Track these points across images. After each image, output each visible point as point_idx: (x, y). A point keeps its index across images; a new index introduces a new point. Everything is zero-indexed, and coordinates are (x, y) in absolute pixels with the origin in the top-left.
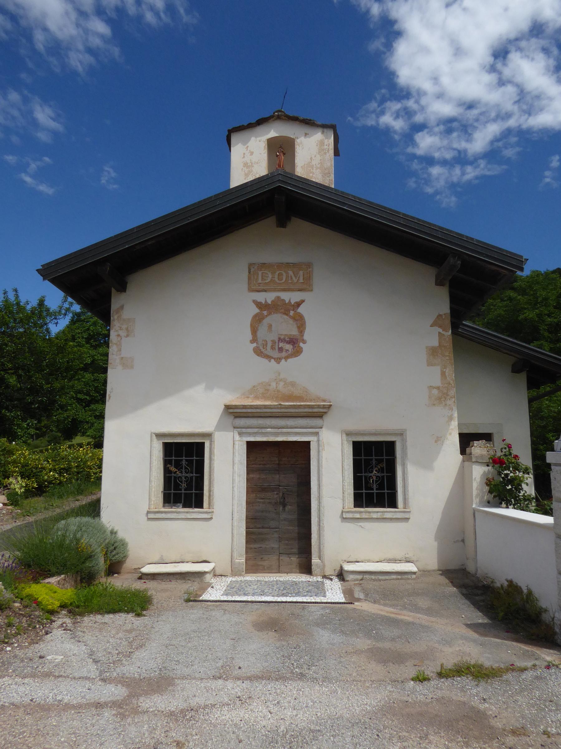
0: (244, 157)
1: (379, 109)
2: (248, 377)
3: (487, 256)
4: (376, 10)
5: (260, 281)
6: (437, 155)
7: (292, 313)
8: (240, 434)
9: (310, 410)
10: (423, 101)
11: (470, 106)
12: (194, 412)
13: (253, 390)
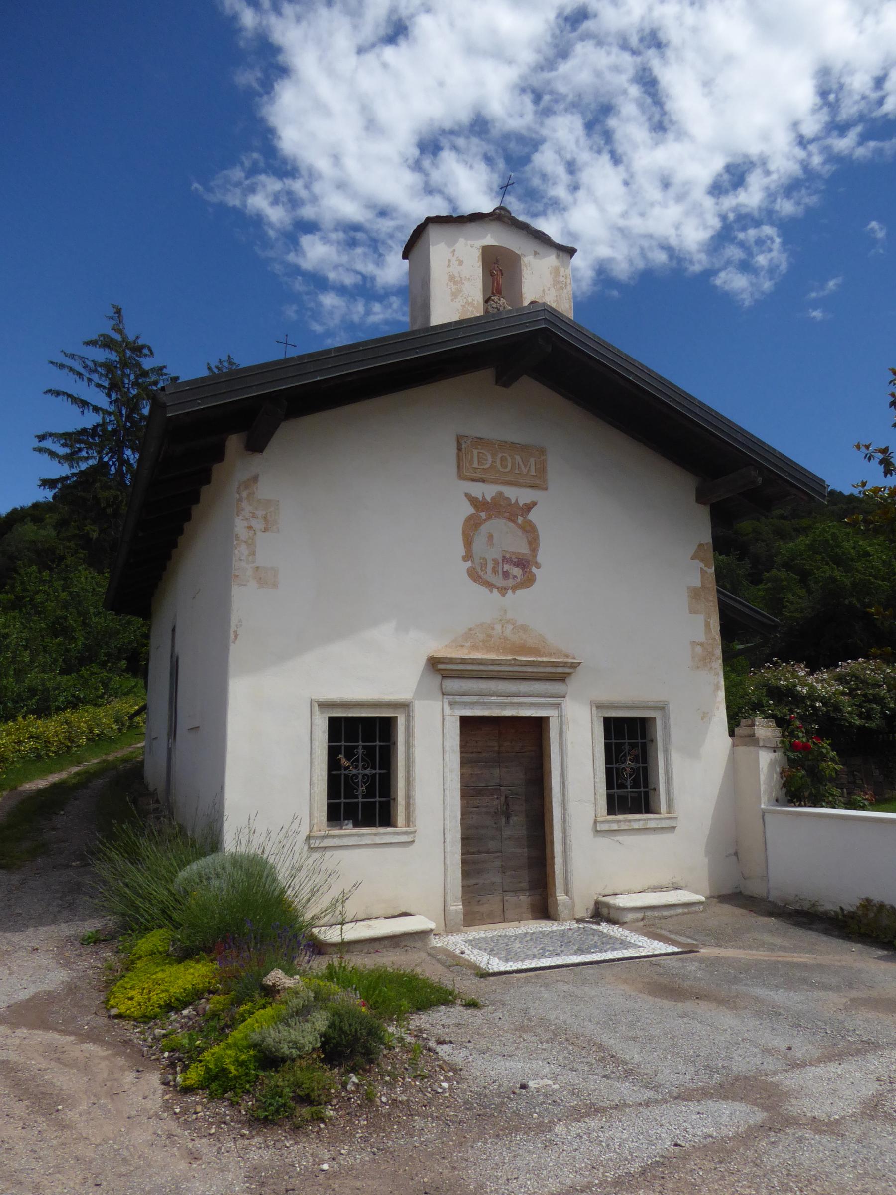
0: (449, 266)
1: (248, 182)
2: (460, 614)
3: (790, 475)
4: (248, 18)
5: (475, 465)
6: (332, 276)
7: (520, 520)
8: (451, 704)
9: (553, 670)
10: (317, 188)
11: (384, 212)
12: (380, 668)
13: (469, 634)
